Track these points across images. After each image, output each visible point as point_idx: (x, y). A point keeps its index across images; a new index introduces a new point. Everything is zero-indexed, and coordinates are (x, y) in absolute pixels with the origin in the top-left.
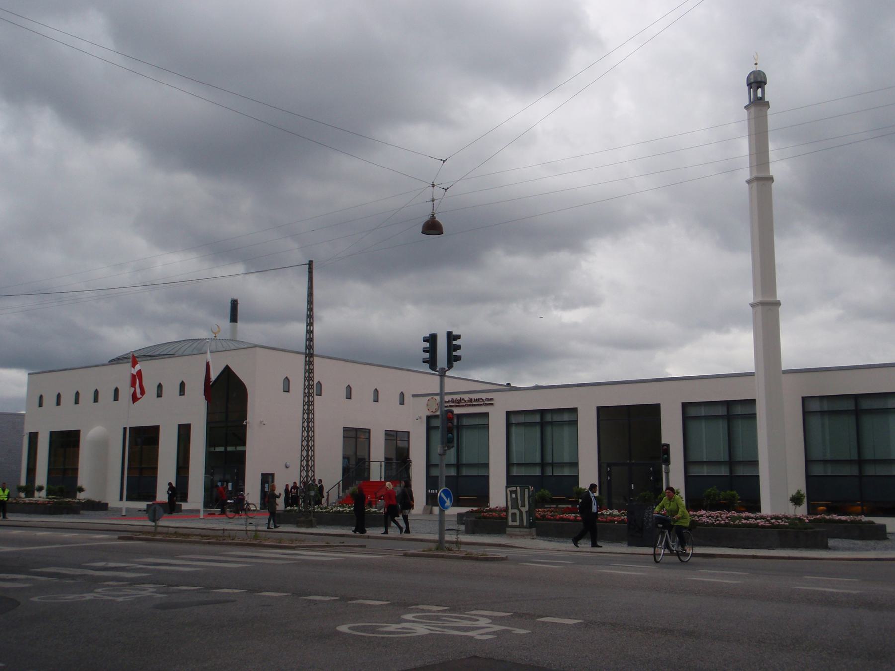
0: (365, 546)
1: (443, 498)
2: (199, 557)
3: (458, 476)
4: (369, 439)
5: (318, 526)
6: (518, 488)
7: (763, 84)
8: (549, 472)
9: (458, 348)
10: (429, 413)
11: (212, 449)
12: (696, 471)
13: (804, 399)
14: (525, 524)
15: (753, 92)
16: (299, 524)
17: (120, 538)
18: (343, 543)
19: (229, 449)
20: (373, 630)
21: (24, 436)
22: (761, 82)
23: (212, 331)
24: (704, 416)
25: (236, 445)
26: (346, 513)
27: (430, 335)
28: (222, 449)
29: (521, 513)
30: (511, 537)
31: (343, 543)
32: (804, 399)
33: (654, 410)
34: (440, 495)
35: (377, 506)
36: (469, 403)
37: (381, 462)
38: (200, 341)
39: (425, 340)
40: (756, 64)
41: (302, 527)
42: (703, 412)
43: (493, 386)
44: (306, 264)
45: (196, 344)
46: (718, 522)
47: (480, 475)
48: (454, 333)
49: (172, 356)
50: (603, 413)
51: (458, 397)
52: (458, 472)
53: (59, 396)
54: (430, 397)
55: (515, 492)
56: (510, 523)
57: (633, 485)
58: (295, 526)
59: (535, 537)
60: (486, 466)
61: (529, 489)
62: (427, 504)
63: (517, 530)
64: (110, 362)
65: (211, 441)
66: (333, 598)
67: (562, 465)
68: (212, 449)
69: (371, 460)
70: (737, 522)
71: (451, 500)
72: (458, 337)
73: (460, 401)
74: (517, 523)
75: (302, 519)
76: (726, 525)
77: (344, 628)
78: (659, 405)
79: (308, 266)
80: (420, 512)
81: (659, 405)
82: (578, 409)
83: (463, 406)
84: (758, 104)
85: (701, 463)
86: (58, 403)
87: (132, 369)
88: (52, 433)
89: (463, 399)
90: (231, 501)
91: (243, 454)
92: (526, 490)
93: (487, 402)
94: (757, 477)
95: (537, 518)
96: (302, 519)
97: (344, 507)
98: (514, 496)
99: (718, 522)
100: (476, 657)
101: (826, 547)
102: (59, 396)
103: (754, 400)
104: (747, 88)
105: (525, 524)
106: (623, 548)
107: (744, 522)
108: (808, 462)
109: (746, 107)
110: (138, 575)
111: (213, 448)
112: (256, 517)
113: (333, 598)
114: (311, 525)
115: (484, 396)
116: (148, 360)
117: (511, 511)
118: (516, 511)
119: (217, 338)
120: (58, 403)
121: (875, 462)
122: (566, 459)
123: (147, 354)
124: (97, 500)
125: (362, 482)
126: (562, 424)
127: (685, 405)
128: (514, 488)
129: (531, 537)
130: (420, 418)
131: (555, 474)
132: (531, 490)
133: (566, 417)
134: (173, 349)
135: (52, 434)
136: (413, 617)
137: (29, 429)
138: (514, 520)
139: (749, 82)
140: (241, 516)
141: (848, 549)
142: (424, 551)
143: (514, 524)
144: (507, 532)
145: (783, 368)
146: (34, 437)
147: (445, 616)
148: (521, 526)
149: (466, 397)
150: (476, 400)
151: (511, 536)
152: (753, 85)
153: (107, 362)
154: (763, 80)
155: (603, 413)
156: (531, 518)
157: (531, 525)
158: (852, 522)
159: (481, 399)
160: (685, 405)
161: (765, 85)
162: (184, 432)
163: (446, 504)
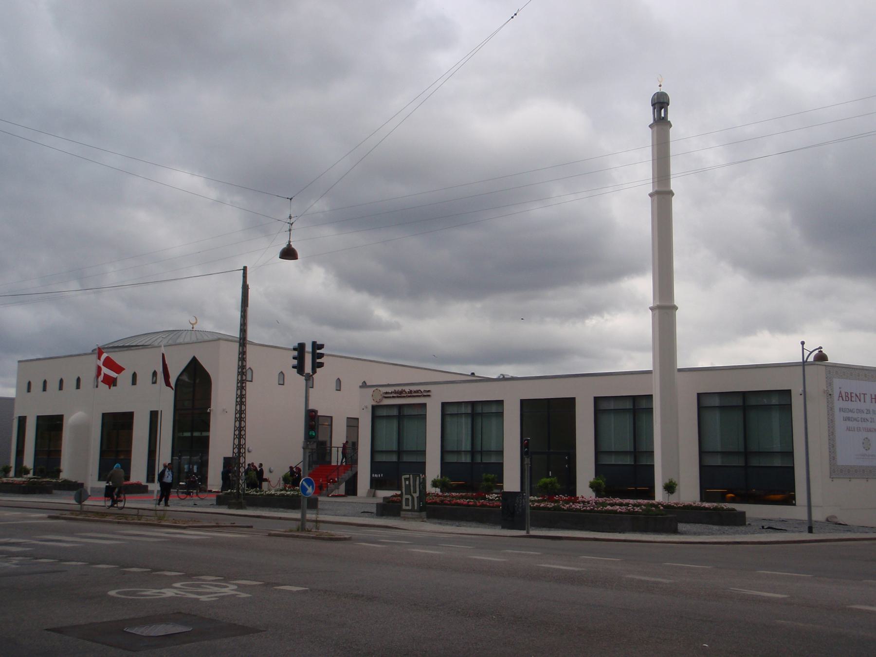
0: (251, 527)
1: (305, 487)
2: (106, 535)
3: (473, 463)
4: (331, 425)
5: (247, 507)
6: (411, 476)
7: (666, 104)
8: (478, 459)
9: (321, 356)
10: (375, 404)
11: (181, 434)
12: (380, 458)
13: (699, 395)
14: (416, 508)
15: (657, 111)
16: (230, 506)
17: (50, 517)
18: (234, 523)
19: (196, 434)
20: (134, 593)
21: (14, 419)
22: (663, 103)
23: (191, 323)
24: (614, 410)
25: (201, 431)
26: (277, 496)
27: (299, 344)
28: (188, 434)
29: (413, 498)
30: (405, 520)
31: (234, 523)
32: (699, 395)
33: (569, 404)
34: (302, 483)
35: (329, 488)
36: (409, 395)
37: (338, 448)
38: (175, 333)
39: (295, 349)
40: (660, 86)
41: (233, 508)
42: (612, 405)
43: (462, 376)
44: (240, 270)
45: (171, 336)
46: (585, 508)
47: (418, 461)
48: (318, 343)
49: (144, 346)
50: (526, 405)
51: (399, 389)
52: (399, 458)
53: (61, 381)
54: (375, 389)
55: (408, 479)
56: (404, 507)
57: (550, 472)
58: (227, 507)
59: (425, 519)
60: (423, 453)
61: (420, 477)
62: (371, 487)
63: (410, 513)
64: (93, 351)
65: (178, 425)
66: (145, 570)
67: (489, 452)
68: (181, 434)
69: (333, 446)
70: (599, 509)
71: (313, 488)
72: (321, 347)
73: (401, 392)
74: (410, 508)
75: (233, 501)
76: (591, 511)
77: (113, 593)
78: (574, 399)
79: (242, 271)
80: (365, 495)
81: (574, 399)
82: (427, 405)
83: (404, 397)
84: (661, 123)
85: (610, 453)
86: (44, 389)
87: (98, 360)
88: (39, 417)
89: (404, 391)
90: (183, 483)
91: (207, 438)
92: (418, 478)
93: (425, 394)
94: (653, 466)
95: (427, 503)
96: (233, 501)
97: (287, 491)
98: (407, 482)
99: (585, 508)
100: (180, 613)
101: (675, 531)
102: (61, 381)
103: (503, 401)
104: (651, 108)
105: (416, 508)
106: (498, 531)
107: (609, 507)
108: (702, 453)
109: (651, 126)
110: (24, 549)
111: (181, 433)
112: (207, 498)
113: (145, 570)
114: (240, 506)
115: (422, 388)
116: (124, 351)
117: (405, 497)
118: (409, 497)
119: (194, 329)
120: (44, 389)
121: (760, 453)
122: (493, 448)
123: (126, 345)
124: (74, 481)
125: (318, 466)
126: (490, 415)
127: (597, 400)
128: (407, 476)
129: (421, 520)
130: (366, 407)
131: (484, 461)
132: (422, 477)
133: (494, 409)
134: (151, 339)
135: (39, 418)
136: (181, 585)
137: (18, 413)
138: (407, 505)
139: (653, 103)
140: (192, 497)
141: (695, 534)
142: (285, 532)
143: (407, 508)
144: (402, 515)
145: (679, 367)
146: (22, 421)
147: (205, 584)
148: (412, 510)
149: (407, 389)
150: (415, 392)
151: (405, 518)
152: (656, 106)
153: (90, 352)
154: (665, 101)
155: (526, 405)
156: (421, 503)
157: (421, 510)
158: (715, 509)
159: (420, 390)
160: (597, 400)
161: (668, 105)
162: (154, 416)
163: (308, 492)
